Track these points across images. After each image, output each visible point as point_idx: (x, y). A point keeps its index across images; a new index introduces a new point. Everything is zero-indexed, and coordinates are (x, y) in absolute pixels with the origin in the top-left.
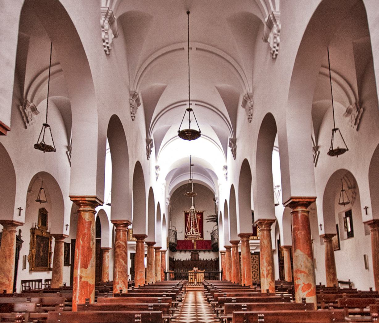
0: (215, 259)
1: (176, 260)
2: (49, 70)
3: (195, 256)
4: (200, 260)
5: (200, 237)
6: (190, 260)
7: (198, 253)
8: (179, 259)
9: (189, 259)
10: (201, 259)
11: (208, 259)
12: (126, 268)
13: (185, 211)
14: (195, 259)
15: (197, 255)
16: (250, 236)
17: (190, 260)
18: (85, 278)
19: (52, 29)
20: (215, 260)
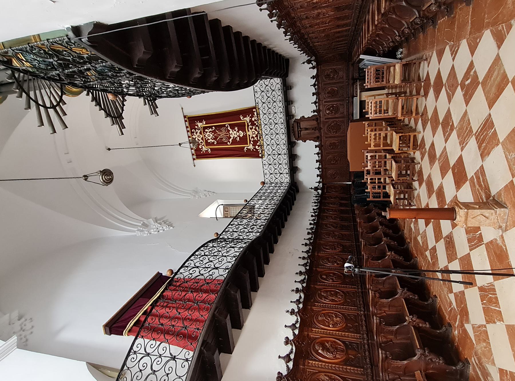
0: (311, 66)
1: (319, 182)
2: (4, 344)
3: (306, 129)
4: (316, 113)
5: (252, 117)
6: (317, 143)
7: (298, 122)
8: (317, 157)
9: (316, 146)
10: (314, 111)
11: (317, 157)
12: (439, 239)
13: (194, 159)
14: (315, 129)
15: (303, 125)
16: (291, 142)
17: (317, 143)
18: (426, 325)
19: (238, 239)
20: (314, 63)
